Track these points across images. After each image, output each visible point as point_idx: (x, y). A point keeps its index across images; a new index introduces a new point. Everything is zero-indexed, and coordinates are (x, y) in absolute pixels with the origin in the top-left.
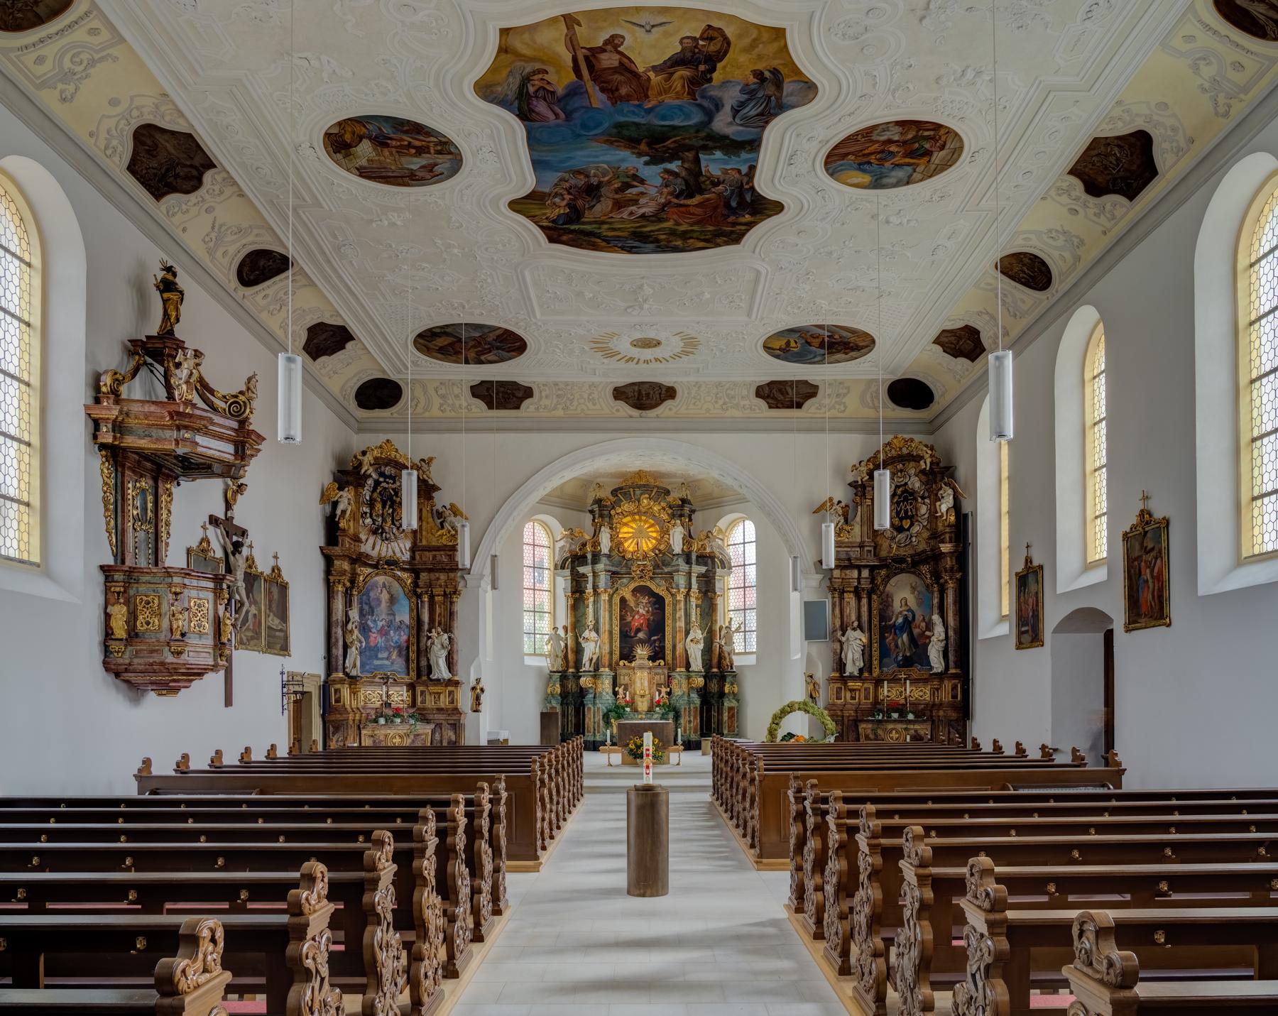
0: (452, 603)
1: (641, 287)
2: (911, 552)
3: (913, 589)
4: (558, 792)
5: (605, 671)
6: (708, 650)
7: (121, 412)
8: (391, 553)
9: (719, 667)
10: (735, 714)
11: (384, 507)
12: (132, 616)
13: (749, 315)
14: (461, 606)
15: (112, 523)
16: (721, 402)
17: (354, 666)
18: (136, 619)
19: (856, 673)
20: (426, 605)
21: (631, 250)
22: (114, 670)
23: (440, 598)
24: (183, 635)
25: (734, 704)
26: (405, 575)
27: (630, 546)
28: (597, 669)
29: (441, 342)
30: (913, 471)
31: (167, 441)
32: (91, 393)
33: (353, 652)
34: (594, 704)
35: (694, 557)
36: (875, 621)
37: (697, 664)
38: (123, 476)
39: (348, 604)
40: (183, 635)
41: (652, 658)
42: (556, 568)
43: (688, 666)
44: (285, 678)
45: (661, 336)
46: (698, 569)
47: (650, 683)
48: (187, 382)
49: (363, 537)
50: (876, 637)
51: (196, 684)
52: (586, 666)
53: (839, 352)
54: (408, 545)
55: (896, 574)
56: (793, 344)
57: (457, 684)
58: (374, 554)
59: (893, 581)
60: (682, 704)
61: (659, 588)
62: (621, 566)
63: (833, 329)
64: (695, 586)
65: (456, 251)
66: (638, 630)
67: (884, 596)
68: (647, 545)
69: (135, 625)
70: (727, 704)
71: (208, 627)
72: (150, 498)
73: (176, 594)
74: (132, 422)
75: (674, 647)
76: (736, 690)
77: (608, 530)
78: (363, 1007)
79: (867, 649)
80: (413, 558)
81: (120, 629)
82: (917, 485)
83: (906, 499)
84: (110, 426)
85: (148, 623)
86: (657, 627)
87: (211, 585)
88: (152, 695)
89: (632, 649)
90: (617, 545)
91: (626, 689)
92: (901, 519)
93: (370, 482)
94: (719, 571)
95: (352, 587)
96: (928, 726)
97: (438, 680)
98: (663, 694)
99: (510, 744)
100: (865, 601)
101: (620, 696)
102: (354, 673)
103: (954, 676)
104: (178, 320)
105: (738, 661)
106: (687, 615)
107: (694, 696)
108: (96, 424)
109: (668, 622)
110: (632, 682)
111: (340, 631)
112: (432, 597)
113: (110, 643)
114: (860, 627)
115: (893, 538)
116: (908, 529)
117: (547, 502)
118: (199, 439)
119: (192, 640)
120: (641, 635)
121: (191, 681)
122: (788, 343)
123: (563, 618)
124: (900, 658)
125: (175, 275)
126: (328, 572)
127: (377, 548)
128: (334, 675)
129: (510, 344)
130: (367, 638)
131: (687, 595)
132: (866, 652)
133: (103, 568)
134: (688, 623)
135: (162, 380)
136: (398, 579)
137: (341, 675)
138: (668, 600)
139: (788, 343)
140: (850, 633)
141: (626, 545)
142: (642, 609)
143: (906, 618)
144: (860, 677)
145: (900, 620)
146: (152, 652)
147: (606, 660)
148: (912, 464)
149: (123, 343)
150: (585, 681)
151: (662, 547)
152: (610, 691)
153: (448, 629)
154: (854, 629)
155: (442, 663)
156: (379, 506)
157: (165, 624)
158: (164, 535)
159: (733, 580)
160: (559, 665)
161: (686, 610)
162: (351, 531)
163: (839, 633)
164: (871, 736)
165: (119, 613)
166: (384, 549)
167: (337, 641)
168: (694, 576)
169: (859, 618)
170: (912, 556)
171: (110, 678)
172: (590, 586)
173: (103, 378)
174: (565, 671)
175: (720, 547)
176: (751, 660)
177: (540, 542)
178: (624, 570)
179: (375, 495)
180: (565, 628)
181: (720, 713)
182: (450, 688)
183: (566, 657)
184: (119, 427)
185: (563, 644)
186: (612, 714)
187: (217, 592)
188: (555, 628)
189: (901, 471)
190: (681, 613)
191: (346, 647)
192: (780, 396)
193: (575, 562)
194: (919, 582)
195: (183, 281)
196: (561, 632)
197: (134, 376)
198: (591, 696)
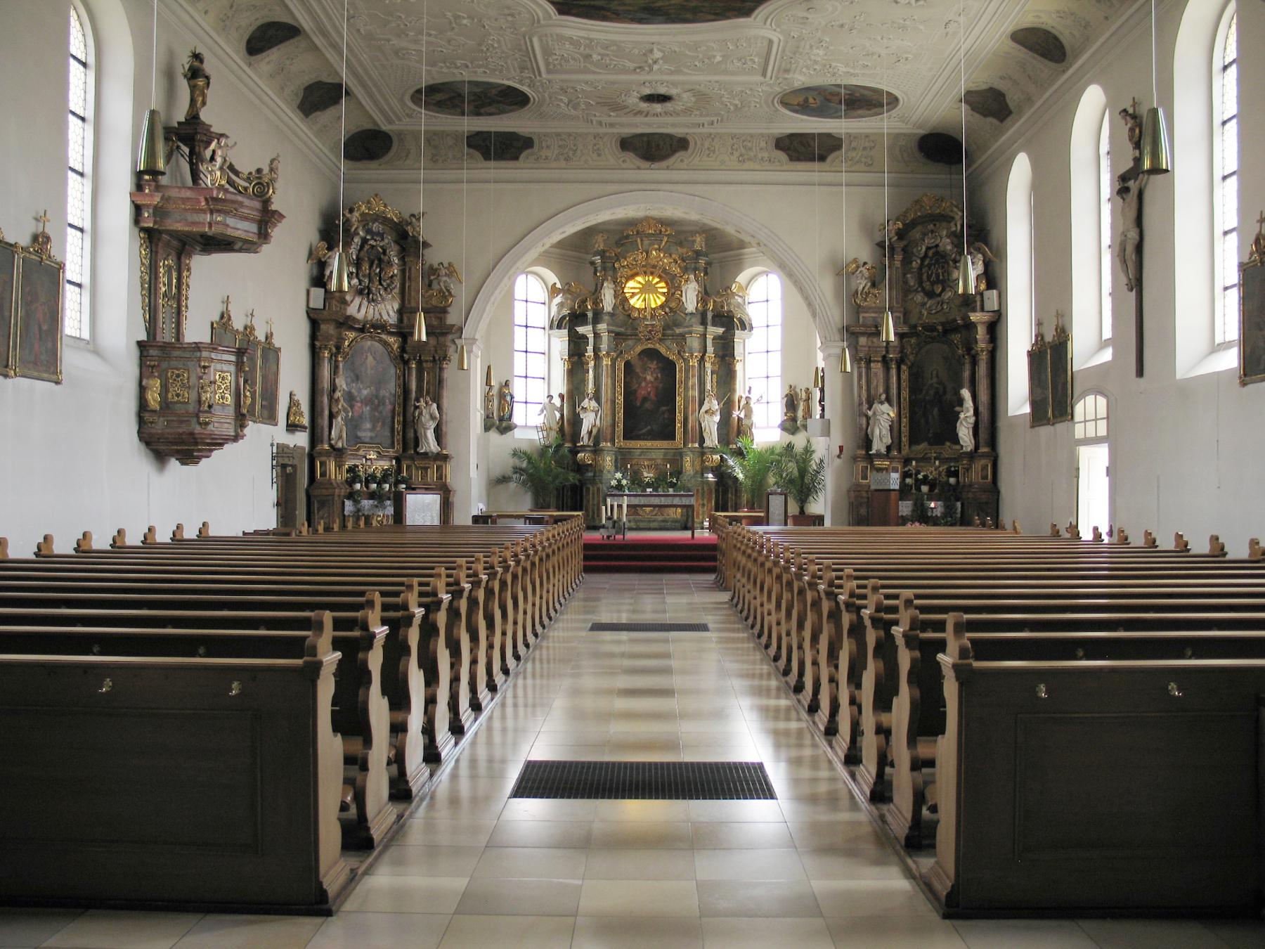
0: (441, 369)
1: (651, 51)
2: (943, 320)
4: (548, 578)
7: (162, 198)
8: (377, 316)
11: (371, 267)
12: (165, 389)
13: (764, 74)
14: (450, 371)
16: (737, 154)
17: (340, 437)
18: (167, 391)
19: (883, 450)
20: (414, 373)
21: (640, 21)
23: (430, 365)
24: (210, 407)
26: (391, 340)
27: (636, 302)
28: (597, 443)
29: (442, 96)
30: (945, 233)
31: (205, 222)
33: (339, 421)
35: (710, 315)
36: (905, 394)
39: (335, 371)
40: (210, 407)
42: (551, 327)
43: (702, 440)
45: (673, 92)
46: (715, 331)
49: (348, 298)
50: (905, 412)
52: (585, 440)
53: (860, 108)
54: (396, 306)
56: (811, 100)
57: (445, 458)
58: (360, 316)
63: (852, 89)
64: (710, 349)
65: (465, 22)
68: (656, 301)
69: (166, 397)
71: (229, 400)
72: (174, 275)
73: (205, 367)
74: (171, 207)
79: (896, 425)
80: (401, 320)
81: (153, 398)
82: (949, 247)
83: (937, 262)
85: (178, 395)
87: (233, 358)
90: (622, 300)
92: (933, 284)
93: (357, 240)
97: (426, 454)
100: (894, 372)
102: (340, 445)
103: (984, 455)
104: (204, 103)
108: (138, 209)
109: (680, 389)
111: (326, 400)
112: (420, 363)
114: (888, 400)
116: (940, 295)
117: (546, 259)
118: (231, 221)
119: (217, 410)
121: (211, 451)
122: (806, 100)
123: (560, 385)
125: (201, 61)
126: (314, 336)
127: (363, 311)
128: (319, 447)
129: (514, 99)
130: (352, 407)
131: (702, 360)
132: (895, 429)
136: (385, 344)
137: (326, 447)
138: (680, 365)
139: (806, 100)
140: (876, 406)
143: (937, 393)
144: (887, 456)
146: (182, 422)
148: (944, 224)
151: (673, 305)
153: (437, 399)
154: (882, 403)
155: (430, 435)
156: (365, 266)
157: (194, 396)
163: (865, 406)
165: (155, 385)
166: (371, 311)
167: (322, 411)
168: (709, 338)
169: (887, 390)
170: (943, 324)
171: (143, 447)
172: (590, 348)
175: (739, 306)
177: (532, 297)
178: (629, 332)
179: (362, 254)
180: (562, 396)
182: (439, 463)
184: (159, 212)
185: (558, 415)
187: (239, 365)
188: (550, 397)
189: (932, 232)
190: (694, 381)
191: (332, 416)
192: (799, 149)
193: (571, 321)
195: (208, 66)
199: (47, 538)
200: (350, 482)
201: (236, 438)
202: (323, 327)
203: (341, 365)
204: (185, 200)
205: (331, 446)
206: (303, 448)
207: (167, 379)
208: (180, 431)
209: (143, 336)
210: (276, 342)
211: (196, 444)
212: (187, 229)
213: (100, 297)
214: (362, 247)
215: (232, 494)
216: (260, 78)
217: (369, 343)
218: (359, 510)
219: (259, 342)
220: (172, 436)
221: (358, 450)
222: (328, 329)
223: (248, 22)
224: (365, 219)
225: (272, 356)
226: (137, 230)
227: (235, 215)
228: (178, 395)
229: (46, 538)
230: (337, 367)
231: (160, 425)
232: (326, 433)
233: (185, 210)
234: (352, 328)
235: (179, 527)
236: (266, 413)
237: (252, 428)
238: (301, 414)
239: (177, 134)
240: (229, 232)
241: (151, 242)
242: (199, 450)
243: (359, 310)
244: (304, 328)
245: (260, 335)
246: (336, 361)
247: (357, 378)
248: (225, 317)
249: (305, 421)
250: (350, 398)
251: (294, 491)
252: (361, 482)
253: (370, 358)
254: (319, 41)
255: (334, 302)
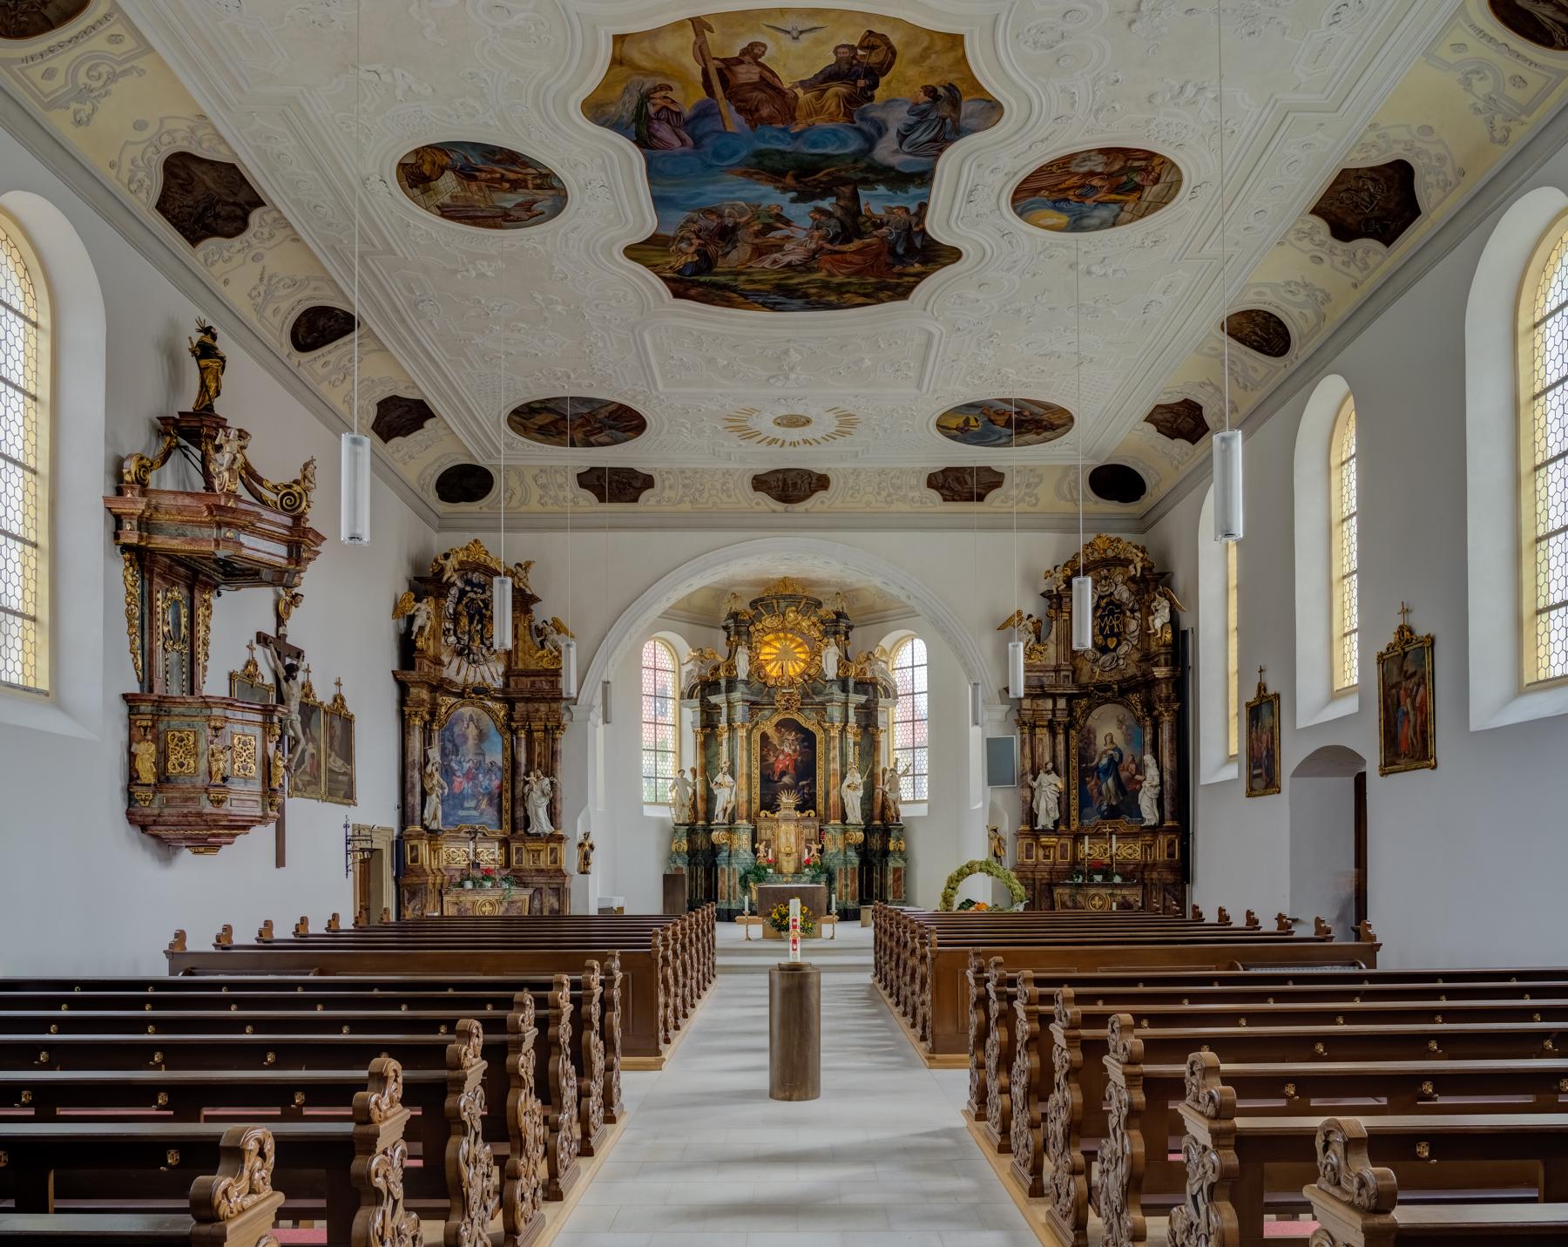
0: (554, 740)
1: (786, 352)
2: (1118, 677)
3: (1121, 722)
4: (685, 972)
5: (743, 823)
6: (868, 798)
7: (148, 505)
8: (479, 679)
9: (882, 819)
10: (902, 876)
11: (471, 623)
12: (163, 756)
13: (919, 387)
14: (565, 743)
15: (138, 641)
16: (884, 494)
17: (435, 817)
18: (166, 759)
19: (1050, 826)
20: (523, 743)
21: (774, 307)
22: (140, 822)
23: (540, 734)
24: (225, 779)
25: (901, 864)
26: (497, 706)
27: (772, 670)
28: (732, 821)
29: (540, 420)
30: (1120, 578)
31: (205, 541)
32: (112, 483)
33: (433, 800)
34: (729, 864)
35: (851, 684)
36: (1074, 763)
37: (855, 815)
38: (151, 584)
39: (427, 741)
40: (225, 779)
41: (801, 808)
42: (682, 697)
43: (844, 817)
44: (350, 832)
45: (812, 413)
46: (857, 699)
47: (797, 838)
48: (229, 469)
49: (445, 659)
50: (1075, 782)
51: (241, 839)
52: (720, 817)
53: (1029, 431)
54: (501, 669)
55: (1099, 705)
56: (972, 422)
57: (560, 839)
58: (459, 679)
59: (1095, 713)
60: (836, 864)
61: (809, 722)
62: (762, 694)
63: (1022, 404)
64: (852, 719)
65: (559, 308)
66: (783, 774)
67: (1084, 732)
68: (794, 669)
69: (166, 768)
70: (892, 864)
71: (255, 770)
72: (184, 611)
73: (216, 729)
74: (161, 518)
75: (827, 794)
76: (903, 847)
77: (746, 650)
78: (446, 1236)
79: (1064, 797)
80: (507, 684)
81: (147, 772)
82: (1126, 595)
83: (1111, 613)
84: (135, 523)
85: (181, 765)
86: (806, 769)
87: (259, 718)
88: (187, 853)
89: (775, 797)
90: (757, 669)
91: (768, 846)
92: (1106, 637)
93: (454, 591)
94: (882, 701)
95: (432, 721)
96: (1139, 891)
97: (538, 835)
98: (814, 852)
99: (626, 913)
100: (1061, 738)
101: (761, 854)
102: (434, 826)
103: (1171, 830)
104: (218, 393)
105: (905, 812)
106: (843, 755)
107: (852, 854)
108: (118, 520)
109: (820, 763)
110: (776, 837)
111: (417, 775)
112: (530, 733)
113: (135, 789)
114: (1055, 770)
115: (1096, 661)
116: (1114, 650)
117: (671, 617)
118: (244, 539)
119: (236, 786)
120: (786, 779)
121: (235, 836)
122: (967, 421)
123: (691, 759)
124: (1104, 808)
125: (214, 337)
126: (402, 702)
127: (463, 672)
128: (410, 829)
129: (626, 422)
130: (450, 783)
131: (843, 730)
132: (1063, 800)
133: (126, 697)
134: (844, 764)
135: (199, 466)
136: (489, 711)
137: (418, 828)
138: (820, 736)
139: (967, 421)
140: (1042, 776)
141: (768, 668)
142: (788, 748)
143: (1111, 759)
144: (1055, 831)
145: (1105, 761)
146: (186, 800)
147: (743, 810)
148: (1119, 569)
149: (151, 421)
150: (718, 836)
151: (812, 671)
152: (749, 848)
153: (550, 772)
154: (1048, 772)
155: (542, 813)
156: (464, 621)
157: (203, 766)
158: (201, 657)
159: (899, 711)
160: (685, 816)
161: (841, 748)
162: (431, 652)
163: (1030, 777)
164: (1069, 904)
165: (147, 752)
166: (472, 674)
167: (413, 786)
168: (852, 707)
169: (1054, 758)
170: (1118, 682)
171: (135, 832)
172: (723, 719)
173: (126, 464)
174: (693, 824)
175: (883, 671)
176: (922, 810)
177: (662, 665)
178: (765, 700)
179: (460, 608)
180: (694, 771)
181: (883, 875)
182: (552, 845)
183: (694, 806)
184: (146, 525)
185: (690, 791)
186: (751, 876)
187: (267, 726)
188: (681, 771)
189: (1106, 578)
190: (835, 753)
191: (424, 794)
192: (957, 486)
193: (705, 690)
194: (1128, 714)
195: (224, 344)
196: (689, 776)
197: (164, 461)
198: (725, 854)
235: (268, 924)
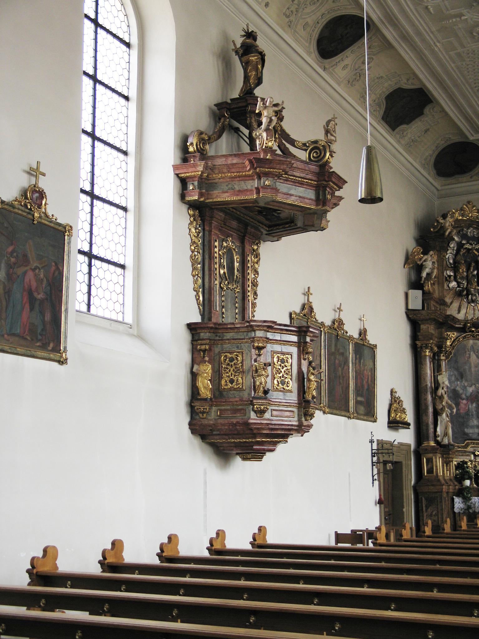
7: (206, 167)
11: (468, 269)
12: (217, 376)
15: (200, 281)
17: (446, 434)
18: (220, 378)
22: (200, 429)
24: (266, 392)
32: (179, 154)
33: (444, 418)
38: (210, 235)
39: (437, 369)
44: (375, 446)
48: (267, 130)
49: (448, 300)
51: (281, 447)
58: (461, 316)
69: (219, 384)
71: (293, 385)
72: (236, 258)
73: (259, 349)
81: (205, 385)
84: (196, 183)
85: (232, 381)
87: (294, 338)
88: (238, 459)
95: (440, 352)
99: (88, 613)
102: (446, 441)
108: (183, 182)
111: (429, 398)
113: (197, 404)
118: (283, 187)
119: (275, 396)
125: (255, 39)
127: (463, 311)
128: (425, 444)
130: (457, 405)
133: (191, 327)
135: (248, 141)
137: (432, 444)
146: (235, 411)
149: (210, 109)
156: (463, 269)
158: (251, 298)
162: (436, 295)
165: (207, 369)
171: (196, 441)
173: (190, 140)
179: (459, 257)
187: (302, 346)
191: (437, 414)
195: (261, 43)
197: (220, 136)
199: (261, 529)
200: (460, 479)
201: (302, 429)
202: (423, 327)
203: (443, 364)
204: (230, 167)
205: (437, 442)
206: (409, 446)
207: (220, 363)
208: (234, 421)
209: (197, 318)
210: (371, 338)
211: (254, 436)
212: (235, 198)
213: (133, 269)
214: (458, 251)
215: (318, 490)
216: (339, 84)
217: (471, 342)
218: (469, 507)
219: (351, 337)
220: (229, 428)
221: (467, 445)
222: (429, 328)
223: (316, 17)
224: (458, 225)
225: (366, 352)
226: (184, 208)
227: (287, 180)
228: (232, 381)
229: (260, 529)
230: (439, 366)
231: (213, 415)
232: (431, 430)
233: (232, 178)
234: (452, 328)
236: (362, 409)
237: (321, 420)
238: (403, 411)
239: (229, 109)
240: (280, 198)
241: (203, 220)
242: (262, 443)
243: (459, 311)
244: (403, 330)
245: (352, 330)
246: (439, 360)
247: (461, 376)
248: (308, 309)
249: (410, 417)
250: (455, 396)
251: (401, 489)
252: (470, 478)
253: (473, 357)
254: (389, 33)
255: (432, 303)
